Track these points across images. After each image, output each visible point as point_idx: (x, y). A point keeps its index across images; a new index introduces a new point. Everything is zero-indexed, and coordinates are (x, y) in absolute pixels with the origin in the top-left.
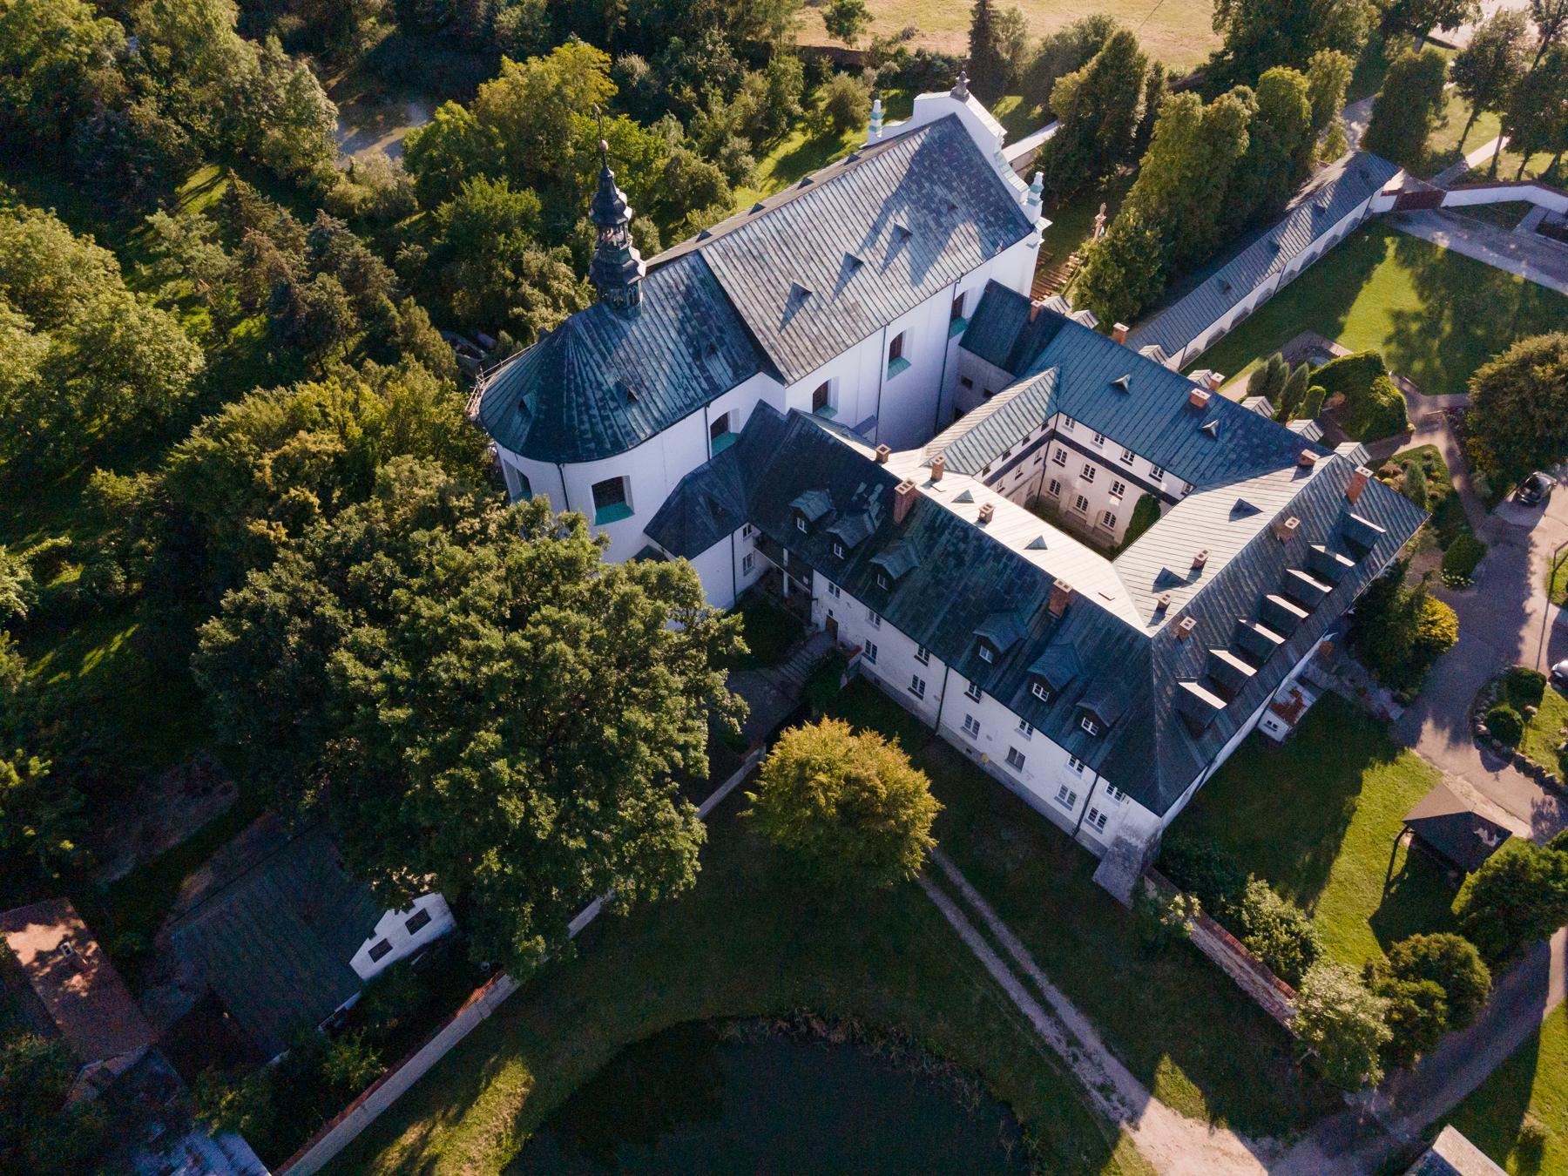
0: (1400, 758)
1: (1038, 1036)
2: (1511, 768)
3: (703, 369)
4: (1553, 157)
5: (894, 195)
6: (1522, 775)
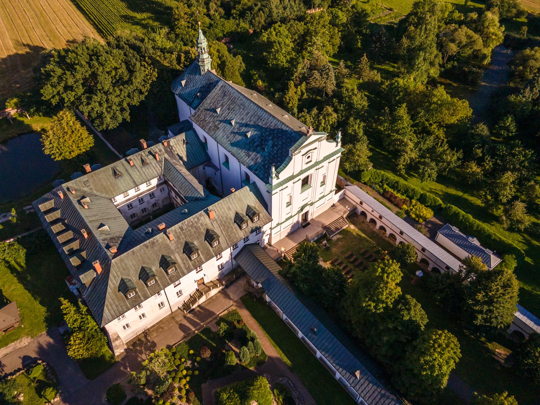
0: (45, 324)
1: (26, 205)
2: (21, 367)
3: (195, 98)
4: (182, 136)
5: (262, 128)
6: (16, 369)
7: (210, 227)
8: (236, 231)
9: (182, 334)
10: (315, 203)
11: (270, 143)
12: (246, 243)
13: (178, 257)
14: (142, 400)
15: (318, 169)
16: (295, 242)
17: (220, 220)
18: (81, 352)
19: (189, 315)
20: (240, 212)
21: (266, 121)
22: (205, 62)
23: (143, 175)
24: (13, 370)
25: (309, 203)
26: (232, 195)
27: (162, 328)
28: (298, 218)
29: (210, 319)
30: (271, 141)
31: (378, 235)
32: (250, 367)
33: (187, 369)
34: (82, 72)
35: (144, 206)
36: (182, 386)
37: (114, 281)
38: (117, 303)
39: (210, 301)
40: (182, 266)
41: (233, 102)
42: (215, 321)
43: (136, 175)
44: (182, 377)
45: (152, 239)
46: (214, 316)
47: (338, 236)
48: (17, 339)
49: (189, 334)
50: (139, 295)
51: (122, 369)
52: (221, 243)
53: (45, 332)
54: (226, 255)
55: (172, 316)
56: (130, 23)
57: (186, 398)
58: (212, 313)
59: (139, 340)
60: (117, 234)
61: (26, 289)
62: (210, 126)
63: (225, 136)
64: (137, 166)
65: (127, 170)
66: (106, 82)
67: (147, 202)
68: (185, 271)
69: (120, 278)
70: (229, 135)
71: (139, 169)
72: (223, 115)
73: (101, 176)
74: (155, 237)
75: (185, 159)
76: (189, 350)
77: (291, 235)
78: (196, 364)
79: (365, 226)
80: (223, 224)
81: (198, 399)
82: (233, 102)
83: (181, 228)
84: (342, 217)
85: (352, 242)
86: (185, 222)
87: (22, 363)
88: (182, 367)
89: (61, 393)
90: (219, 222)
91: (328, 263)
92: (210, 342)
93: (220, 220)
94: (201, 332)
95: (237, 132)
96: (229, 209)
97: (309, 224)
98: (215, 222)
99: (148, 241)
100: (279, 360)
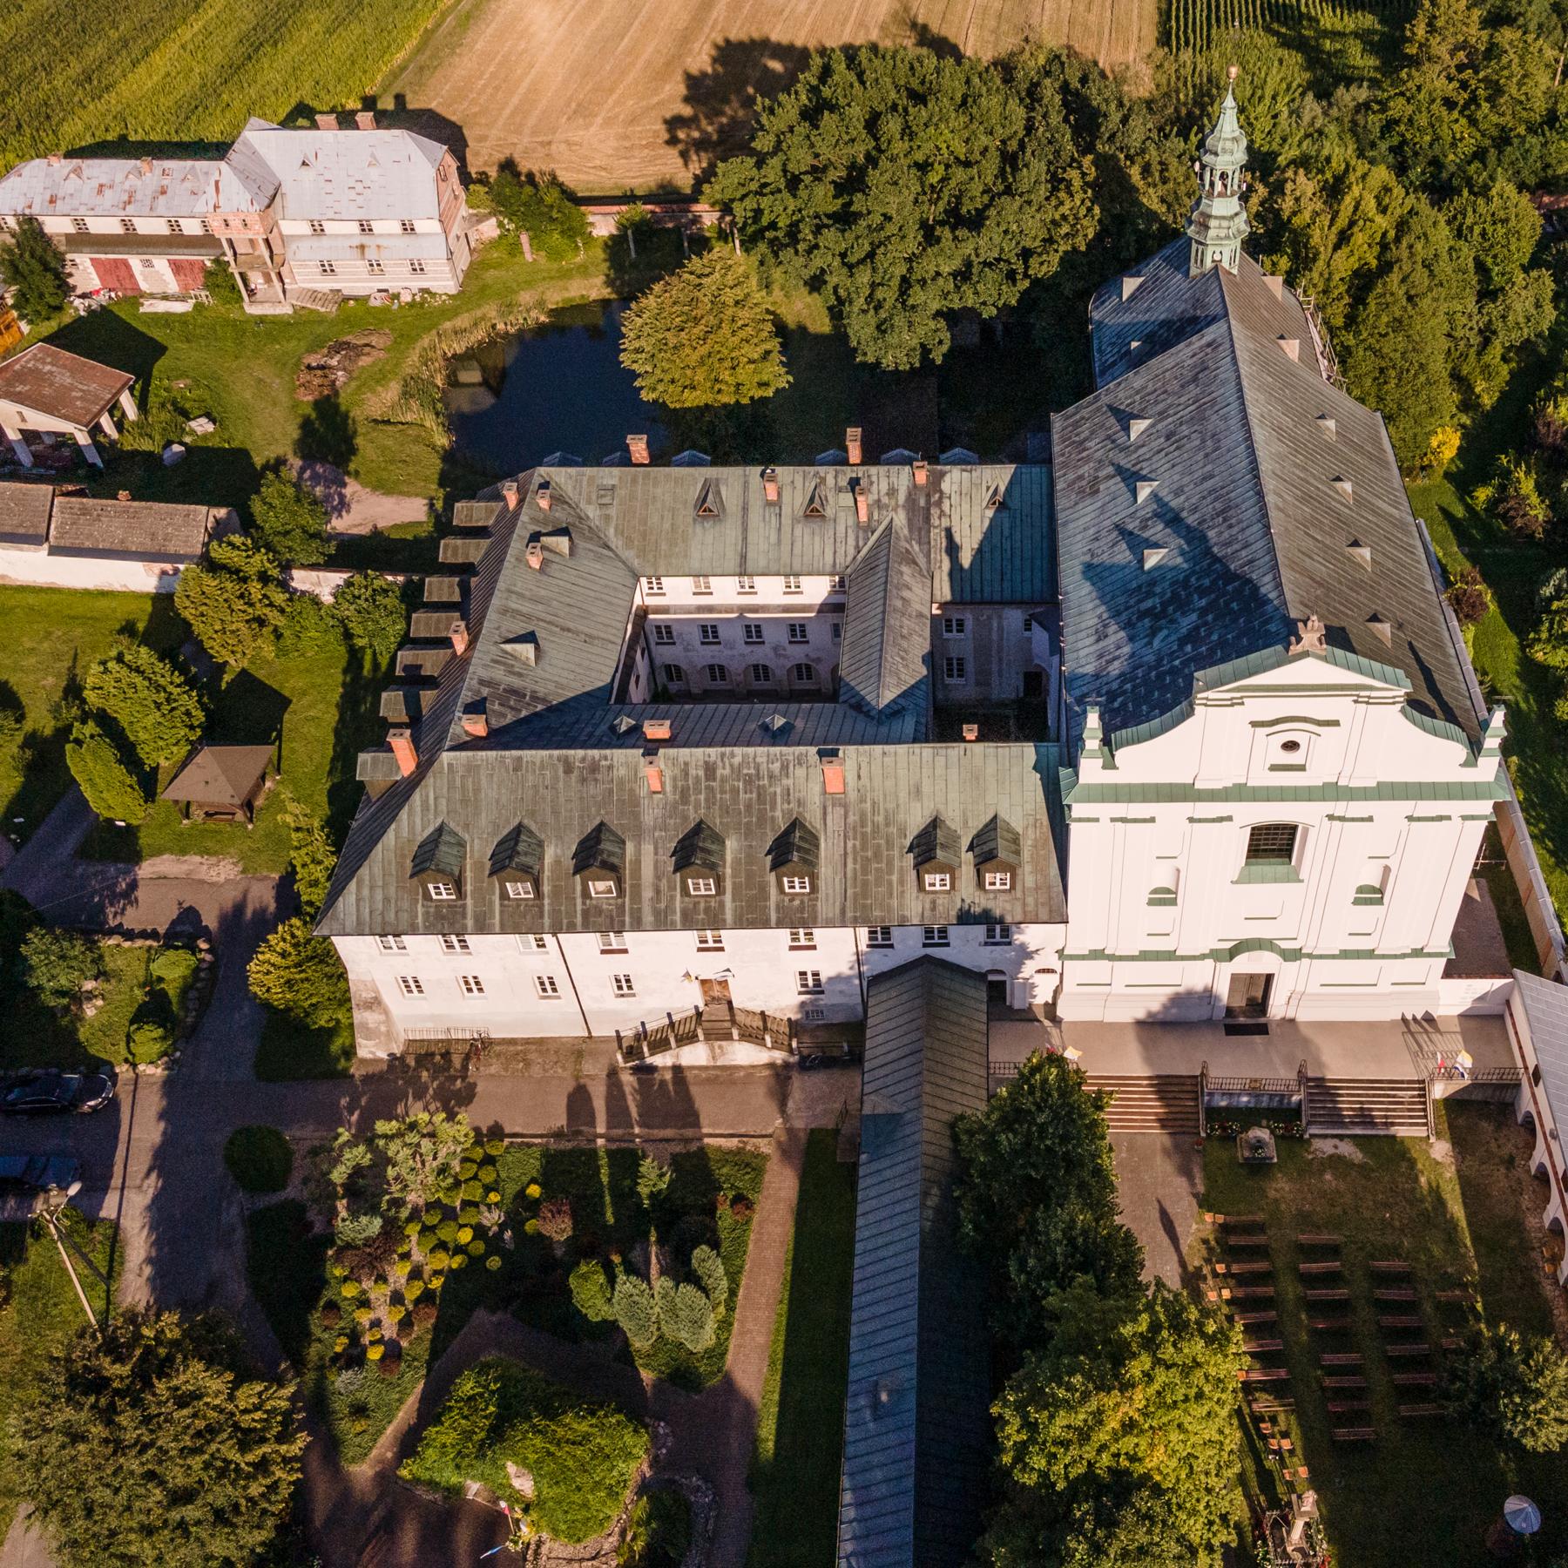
2: (162, 931)
4: (999, 476)
5: (1208, 552)
7: (813, 818)
8: (902, 882)
9: (560, 1120)
10: (1310, 956)
11: (1187, 622)
12: (929, 951)
13: (647, 858)
14: (310, 1225)
15: (1342, 819)
16: (1148, 1060)
17: (863, 815)
18: (269, 981)
19: (628, 1079)
20: (953, 819)
21: (1235, 530)
22: (1212, 233)
23: (786, 548)
24: (142, 927)
25: (1284, 945)
26: (955, 750)
27: (528, 1063)
28: (1219, 980)
29: (669, 1133)
30: (1194, 616)
31: (1525, 1247)
32: (646, 1366)
33: (480, 1231)
34: (837, 142)
35: (761, 655)
36: (427, 1270)
37: (418, 821)
38: (392, 890)
39: (723, 1077)
40: (647, 894)
41: (1199, 417)
42: (678, 1148)
43: (762, 534)
44: (451, 1245)
45: (595, 753)
46: (689, 1132)
47: (1346, 1149)
48: (215, 854)
49: (579, 1133)
50: (464, 906)
51: (344, 1102)
52: (821, 894)
53: (276, 876)
54: (838, 951)
55: (580, 1049)
56: (1277, 34)
57: (409, 1314)
58: (690, 1117)
59: (446, 1055)
60: (542, 691)
61: (337, 732)
62: (1081, 472)
63: (1092, 531)
64: (786, 510)
65: (745, 509)
66: (894, 199)
67: (775, 649)
68: (648, 918)
69: (439, 821)
70: (1104, 533)
71: (786, 521)
72: (1141, 451)
73: (659, 491)
74: (608, 752)
75: (966, 559)
76: (533, 1181)
77: (1154, 1028)
78: (508, 1235)
79: (1499, 1179)
80: (867, 838)
81: (433, 1341)
82: (1199, 417)
83: (710, 770)
84: (1422, 1087)
85: (1387, 1206)
86: (733, 755)
87: (173, 923)
88: (469, 1217)
89: (174, 1062)
90: (852, 818)
91: (1208, 1217)
92: (608, 1198)
93: (863, 815)
94: (610, 1153)
95: (1131, 533)
96: (917, 792)
97: (1263, 1030)
98: (840, 811)
99: (581, 753)
100: (749, 1413)
